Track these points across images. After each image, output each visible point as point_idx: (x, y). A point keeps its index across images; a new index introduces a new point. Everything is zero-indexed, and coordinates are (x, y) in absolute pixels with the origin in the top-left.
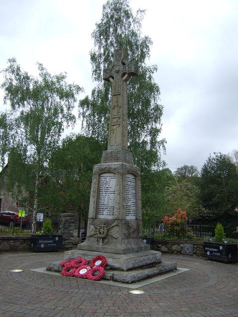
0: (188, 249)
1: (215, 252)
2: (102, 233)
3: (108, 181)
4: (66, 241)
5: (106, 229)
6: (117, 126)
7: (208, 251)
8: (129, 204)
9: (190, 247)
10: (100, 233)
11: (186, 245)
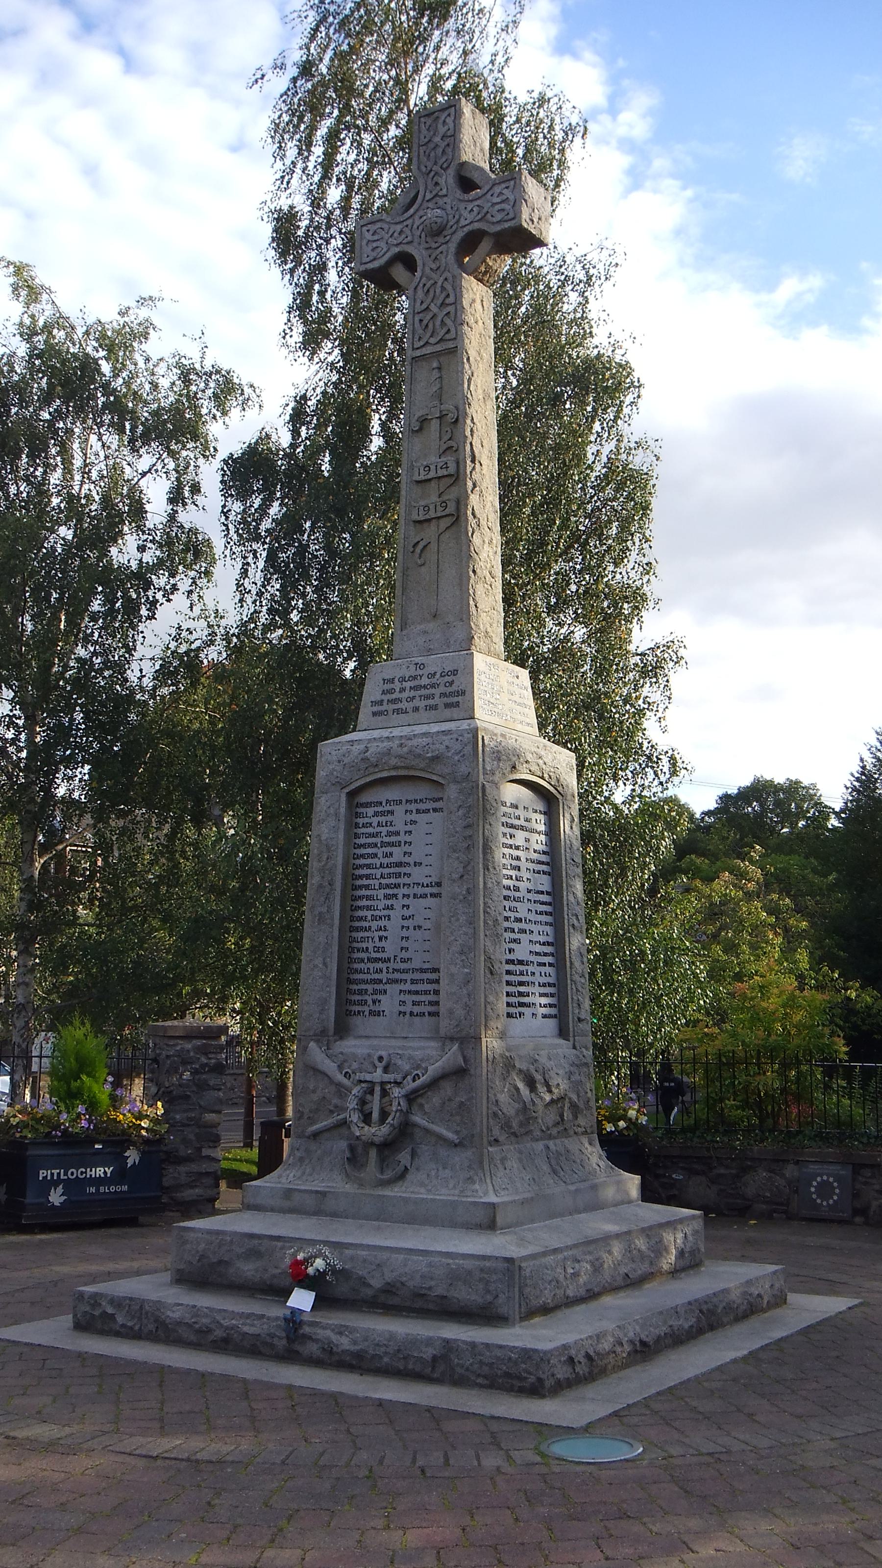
0: (825, 1189)
1: (98, 1181)
2: (375, 1115)
3: (400, 826)
4: (183, 1169)
5: (396, 1092)
6: (444, 523)
7: (55, 1183)
8: (521, 952)
9: (838, 1179)
10: (367, 1118)
11: (813, 1168)
